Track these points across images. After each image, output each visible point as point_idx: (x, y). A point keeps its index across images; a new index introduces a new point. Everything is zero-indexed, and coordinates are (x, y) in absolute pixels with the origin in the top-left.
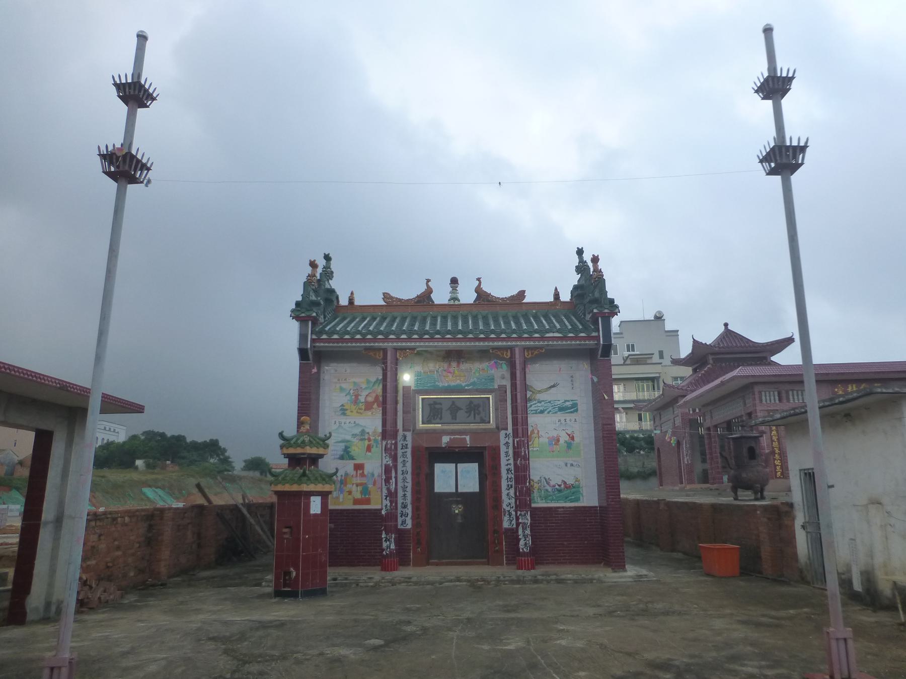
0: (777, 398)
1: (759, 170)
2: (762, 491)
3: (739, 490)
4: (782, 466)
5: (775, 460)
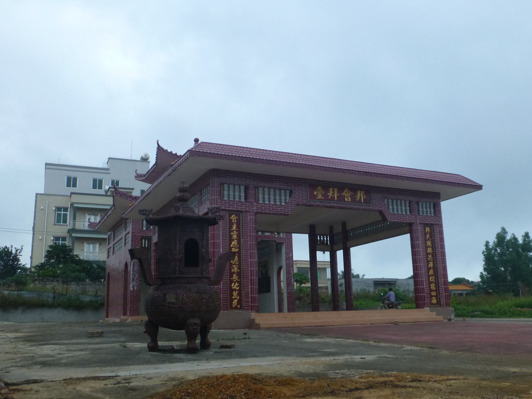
0: (243, 194)
2: (204, 331)
3: (162, 330)
4: (240, 291)
5: (231, 282)
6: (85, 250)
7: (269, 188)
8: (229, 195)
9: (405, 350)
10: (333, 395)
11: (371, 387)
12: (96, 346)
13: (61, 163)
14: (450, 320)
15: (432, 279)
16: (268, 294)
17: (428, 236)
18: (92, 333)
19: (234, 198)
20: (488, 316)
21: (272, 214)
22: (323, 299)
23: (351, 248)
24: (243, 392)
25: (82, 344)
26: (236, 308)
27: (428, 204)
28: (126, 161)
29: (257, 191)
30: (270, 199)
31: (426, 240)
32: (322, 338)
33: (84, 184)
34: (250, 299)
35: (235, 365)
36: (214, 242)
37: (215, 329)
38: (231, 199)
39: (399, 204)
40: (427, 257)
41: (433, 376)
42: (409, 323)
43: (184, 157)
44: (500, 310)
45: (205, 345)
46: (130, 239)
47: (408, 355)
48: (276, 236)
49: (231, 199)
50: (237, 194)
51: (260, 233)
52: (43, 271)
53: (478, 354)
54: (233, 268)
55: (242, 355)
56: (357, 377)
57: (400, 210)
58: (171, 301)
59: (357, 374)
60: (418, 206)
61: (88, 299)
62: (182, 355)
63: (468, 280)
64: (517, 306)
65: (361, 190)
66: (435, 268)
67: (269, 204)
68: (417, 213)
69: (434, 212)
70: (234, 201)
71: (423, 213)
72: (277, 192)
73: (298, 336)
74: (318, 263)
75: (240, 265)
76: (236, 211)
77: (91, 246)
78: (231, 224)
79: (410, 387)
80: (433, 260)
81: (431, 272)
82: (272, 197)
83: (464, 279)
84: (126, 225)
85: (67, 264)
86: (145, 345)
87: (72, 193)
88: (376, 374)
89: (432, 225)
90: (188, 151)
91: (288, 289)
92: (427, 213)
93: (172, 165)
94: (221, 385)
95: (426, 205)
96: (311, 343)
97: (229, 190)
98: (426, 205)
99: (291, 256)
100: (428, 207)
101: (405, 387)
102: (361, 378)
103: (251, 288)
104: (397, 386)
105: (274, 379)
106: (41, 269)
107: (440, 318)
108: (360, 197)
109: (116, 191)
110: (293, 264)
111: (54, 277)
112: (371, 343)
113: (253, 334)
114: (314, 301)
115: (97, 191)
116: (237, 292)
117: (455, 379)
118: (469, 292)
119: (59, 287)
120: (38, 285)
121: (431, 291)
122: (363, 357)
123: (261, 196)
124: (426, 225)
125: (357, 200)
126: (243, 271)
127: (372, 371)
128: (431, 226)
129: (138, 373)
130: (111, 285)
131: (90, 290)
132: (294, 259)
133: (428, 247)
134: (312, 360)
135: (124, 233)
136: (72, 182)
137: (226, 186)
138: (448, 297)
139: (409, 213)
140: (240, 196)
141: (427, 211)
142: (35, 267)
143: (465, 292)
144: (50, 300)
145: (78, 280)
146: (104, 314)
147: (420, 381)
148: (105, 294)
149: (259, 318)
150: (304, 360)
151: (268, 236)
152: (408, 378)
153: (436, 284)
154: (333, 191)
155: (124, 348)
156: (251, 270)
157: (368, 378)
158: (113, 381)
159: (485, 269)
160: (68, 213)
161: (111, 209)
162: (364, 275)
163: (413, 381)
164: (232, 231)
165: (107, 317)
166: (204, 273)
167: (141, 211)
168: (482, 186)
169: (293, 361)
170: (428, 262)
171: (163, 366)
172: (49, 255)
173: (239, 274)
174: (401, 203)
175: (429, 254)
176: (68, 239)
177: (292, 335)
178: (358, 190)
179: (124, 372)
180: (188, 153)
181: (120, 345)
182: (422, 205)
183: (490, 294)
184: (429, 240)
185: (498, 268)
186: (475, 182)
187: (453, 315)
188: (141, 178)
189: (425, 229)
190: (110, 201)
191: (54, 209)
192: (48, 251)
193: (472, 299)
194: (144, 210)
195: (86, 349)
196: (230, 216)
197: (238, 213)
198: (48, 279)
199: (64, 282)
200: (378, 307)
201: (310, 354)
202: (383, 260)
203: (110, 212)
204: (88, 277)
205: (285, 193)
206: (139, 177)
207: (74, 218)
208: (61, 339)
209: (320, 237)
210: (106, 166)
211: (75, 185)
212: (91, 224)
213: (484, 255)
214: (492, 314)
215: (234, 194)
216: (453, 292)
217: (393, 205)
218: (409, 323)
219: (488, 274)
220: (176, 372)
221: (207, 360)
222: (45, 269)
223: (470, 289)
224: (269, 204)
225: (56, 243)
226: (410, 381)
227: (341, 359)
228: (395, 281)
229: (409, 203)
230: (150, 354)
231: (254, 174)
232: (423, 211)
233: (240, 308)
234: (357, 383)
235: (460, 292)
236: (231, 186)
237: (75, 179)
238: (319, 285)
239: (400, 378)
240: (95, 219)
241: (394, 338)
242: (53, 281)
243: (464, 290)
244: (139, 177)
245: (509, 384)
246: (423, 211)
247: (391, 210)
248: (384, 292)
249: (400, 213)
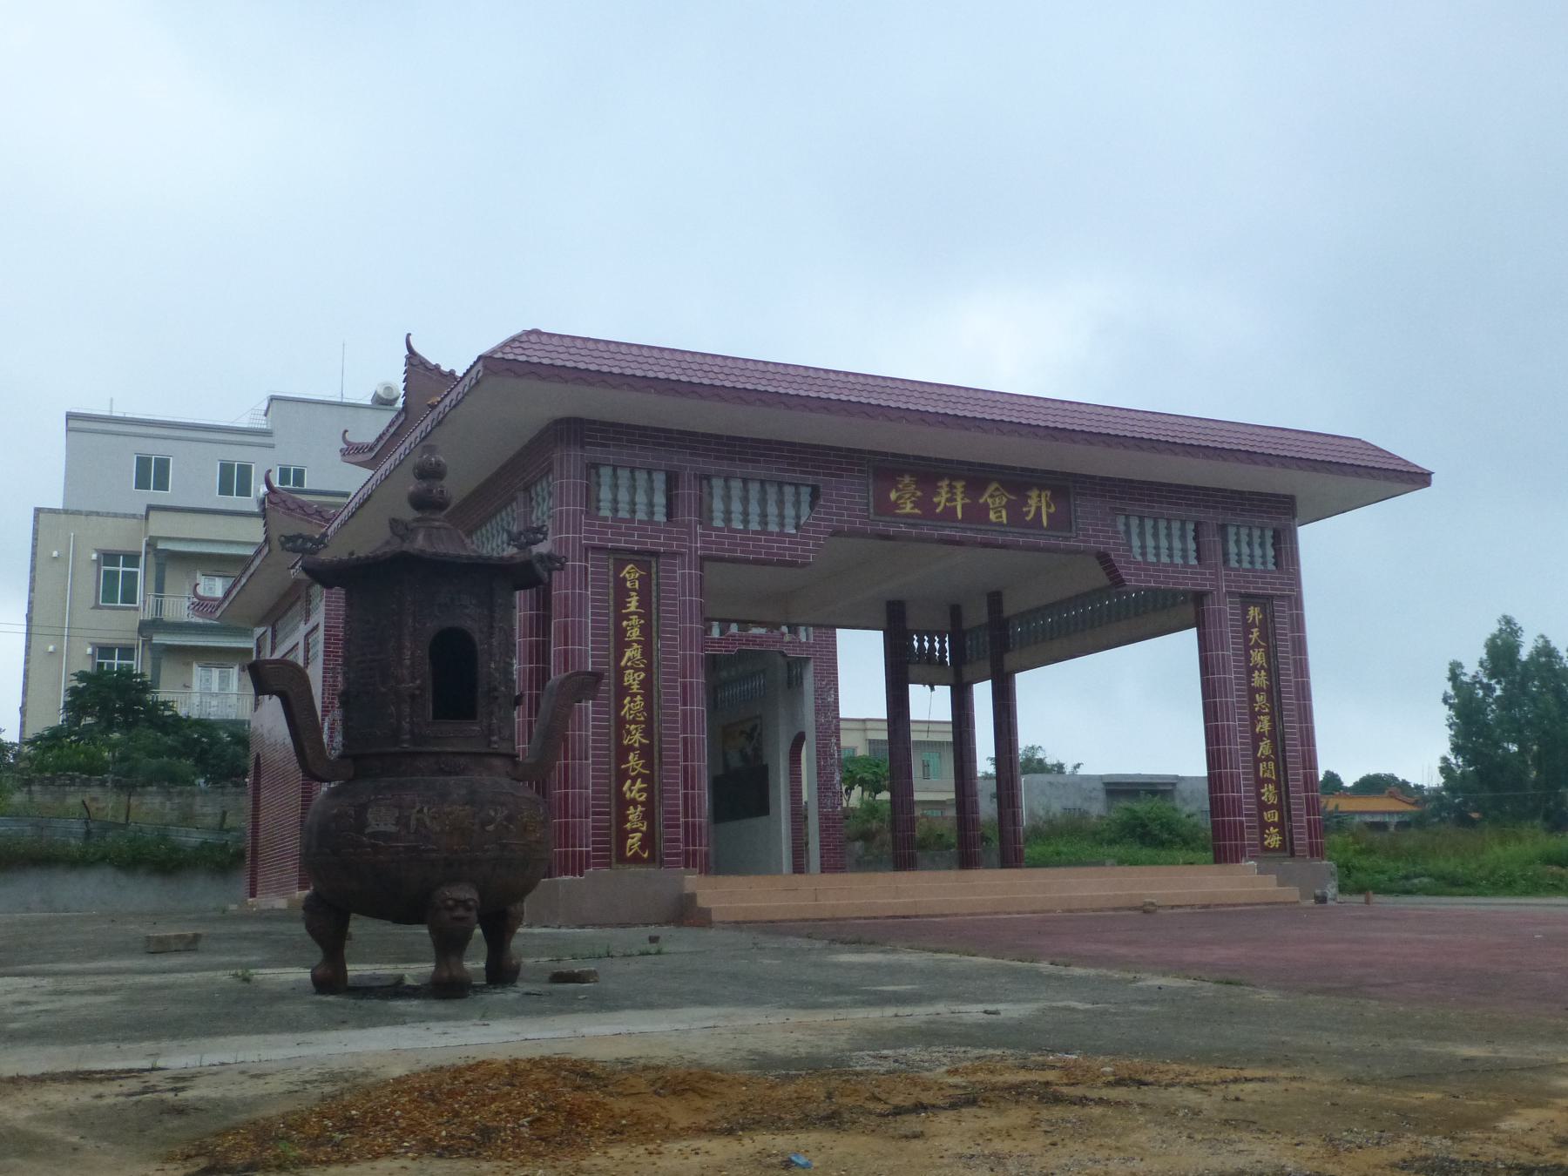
0: (660, 499)
1: (1499, 616)
2: (499, 926)
3: (360, 927)
4: (649, 804)
5: (622, 776)
6: (196, 685)
7: (745, 481)
8: (615, 501)
9: (1140, 989)
10: (832, 1125)
11: (971, 1102)
12: (156, 979)
13: (117, 413)
14: (1322, 900)
15: (1267, 770)
16: (764, 818)
17: (1255, 633)
18: (160, 940)
19: (633, 512)
20: (1454, 890)
21: (756, 562)
22: (941, 836)
23: (1017, 676)
24: (527, 1115)
25: (97, 973)
26: (636, 859)
27: (1256, 533)
28: (326, 408)
29: (706, 490)
30: (742, 511)
31: (1248, 649)
32: (894, 951)
33: (193, 480)
34: (681, 830)
35: (565, 1033)
36: (566, 651)
37: (568, 927)
38: (623, 514)
39: (1163, 532)
40: (1253, 700)
41: (1193, 1069)
42: (1188, 910)
43: (467, 380)
44: (1492, 873)
45: (501, 973)
46: (320, 647)
47: (1144, 1002)
48: (787, 638)
49: (623, 514)
50: (641, 498)
51: (734, 628)
52: (56, 751)
53: (1374, 1003)
54: (629, 732)
55: (604, 1003)
56: (944, 1068)
57: (1164, 552)
58: (382, 828)
59: (945, 1060)
60: (1225, 541)
61: (193, 838)
62: (415, 1002)
63: (1405, 783)
64: (1549, 861)
65: (1041, 488)
66: (1277, 737)
67: (746, 530)
68: (1220, 560)
69: (1275, 557)
70: (632, 520)
71: (1239, 561)
72: (772, 492)
73: (818, 945)
74: (913, 727)
75: (649, 721)
76: (638, 552)
77: (215, 673)
78: (622, 593)
79: (1100, 1101)
80: (1271, 709)
81: (1265, 748)
82: (754, 508)
83: (1392, 778)
84: (309, 602)
85: (134, 732)
86: (305, 974)
87: (150, 508)
88: (1010, 1061)
90: (480, 358)
91: (821, 805)
92: (1252, 562)
93: (433, 407)
94: (463, 1094)
95: (1250, 535)
96: (851, 967)
97: (615, 487)
98: (1250, 535)
99: (831, 700)
100: (1256, 541)
101: (1083, 1101)
102: (954, 1072)
103: (686, 795)
104: (1058, 1099)
105: (652, 1075)
106: (50, 748)
107: (1291, 893)
108: (1039, 509)
109: (283, 501)
110: (838, 729)
111: (91, 770)
112: (1044, 966)
113: (679, 941)
114: (900, 842)
115: (234, 502)
116: (640, 808)
117: (1262, 1080)
118: (1407, 818)
119: (106, 803)
120: (40, 795)
121: (1263, 807)
122: (990, 1008)
123: (718, 505)
124: (1248, 599)
125: (1028, 518)
126: (660, 741)
127: (999, 1052)
128: (1264, 601)
129: (228, 1058)
130: (264, 794)
131: (206, 811)
132: (844, 713)
133: (1255, 668)
134: (823, 1017)
135: (303, 629)
136: (152, 473)
137: (606, 473)
138: (1316, 829)
139: (1193, 562)
140: (651, 505)
141: (1251, 556)
142: (31, 743)
143: (1396, 819)
144: (73, 841)
145: (169, 780)
146: (244, 887)
147: (1141, 1083)
148: (247, 825)
149: (716, 893)
150: (798, 1016)
151: (760, 636)
152: (1104, 1074)
153: (1278, 787)
154: (951, 487)
155: (246, 985)
156: (685, 739)
157: (975, 1072)
158: (133, 1084)
159: (1457, 749)
160: (140, 571)
161: (258, 553)
162: (1078, 766)
163: (1119, 1082)
164: (627, 617)
165: (253, 895)
166: (495, 738)
167: (289, 539)
168: (1430, 474)
169: (763, 1020)
170: (1254, 717)
171: (332, 1035)
172: (78, 702)
173: (646, 752)
174: (1169, 528)
175: (1259, 690)
176: (138, 654)
177: (804, 943)
178: (1030, 486)
179: (179, 1058)
180: (480, 366)
181: (236, 975)
182: (1237, 534)
183: (1473, 823)
184: (1257, 645)
185: (1497, 745)
186: (1407, 463)
187: (1335, 883)
188: (360, 458)
189: (1245, 613)
190: (254, 531)
191: (94, 556)
192: (73, 691)
193: (1411, 839)
194: (300, 536)
195: (114, 990)
196: (620, 566)
197: (644, 558)
198: (72, 779)
199: (119, 786)
200: (1108, 862)
201: (829, 1000)
202: (1116, 714)
203: (257, 562)
204: (203, 774)
205: (797, 494)
206: (352, 452)
207: (160, 588)
208: (60, 958)
209: (921, 641)
210: (261, 423)
211: (162, 484)
212: (202, 604)
213: (1451, 706)
214: (1469, 884)
215: (632, 498)
216: (1357, 819)
217: (1142, 535)
218: (1188, 910)
219: (1468, 763)
220: (358, 1054)
221: (483, 1016)
222: (61, 748)
223: (1409, 808)
224: (746, 530)
225: (100, 665)
226: (1109, 1084)
227: (919, 1014)
228: (1174, 784)
229: (1196, 530)
230: (312, 1003)
232: (1239, 554)
233: (651, 860)
234: (926, 1089)
235: (1377, 819)
237: (163, 465)
238: (917, 796)
239: (1079, 1072)
240: (215, 588)
241: (1123, 951)
242: (86, 783)
243: (1390, 813)
244: (352, 452)
245: (1439, 1096)
246: (1239, 554)
247: (1136, 550)
248: (1136, 817)
249: (1167, 560)
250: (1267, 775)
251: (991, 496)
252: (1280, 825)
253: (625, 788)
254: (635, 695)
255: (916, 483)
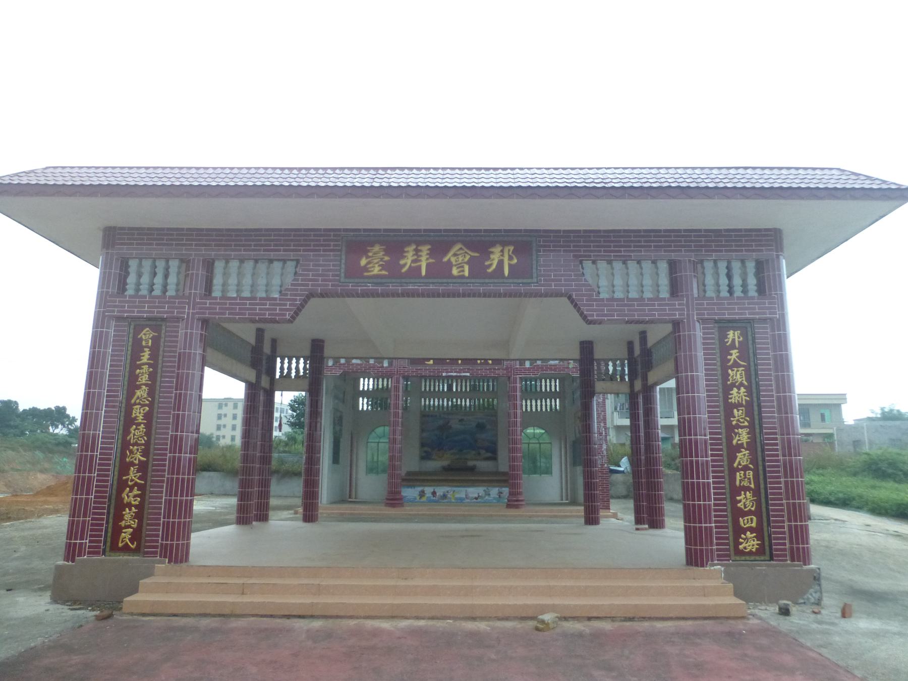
0: (752, 281)
17: (735, 354)
26: (126, 549)
54: (131, 452)
65: (504, 244)
69: (127, 274)
76: (149, 319)
89: (749, 321)
108: (501, 263)
124: (724, 325)
125: (490, 270)
128: (745, 325)
133: (733, 385)
173: (143, 467)
175: (738, 405)
184: (736, 365)
196: (138, 329)
231: (679, 231)
233: (137, 551)
236: (144, 262)
250: (745, 483)
251: (455, 255)
252: (758, 532)
253: (124, 495)
254: (139, 424)
255: (385, 250)
